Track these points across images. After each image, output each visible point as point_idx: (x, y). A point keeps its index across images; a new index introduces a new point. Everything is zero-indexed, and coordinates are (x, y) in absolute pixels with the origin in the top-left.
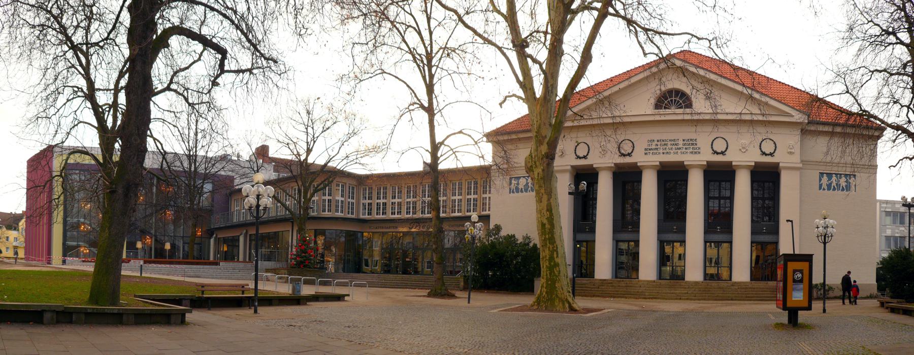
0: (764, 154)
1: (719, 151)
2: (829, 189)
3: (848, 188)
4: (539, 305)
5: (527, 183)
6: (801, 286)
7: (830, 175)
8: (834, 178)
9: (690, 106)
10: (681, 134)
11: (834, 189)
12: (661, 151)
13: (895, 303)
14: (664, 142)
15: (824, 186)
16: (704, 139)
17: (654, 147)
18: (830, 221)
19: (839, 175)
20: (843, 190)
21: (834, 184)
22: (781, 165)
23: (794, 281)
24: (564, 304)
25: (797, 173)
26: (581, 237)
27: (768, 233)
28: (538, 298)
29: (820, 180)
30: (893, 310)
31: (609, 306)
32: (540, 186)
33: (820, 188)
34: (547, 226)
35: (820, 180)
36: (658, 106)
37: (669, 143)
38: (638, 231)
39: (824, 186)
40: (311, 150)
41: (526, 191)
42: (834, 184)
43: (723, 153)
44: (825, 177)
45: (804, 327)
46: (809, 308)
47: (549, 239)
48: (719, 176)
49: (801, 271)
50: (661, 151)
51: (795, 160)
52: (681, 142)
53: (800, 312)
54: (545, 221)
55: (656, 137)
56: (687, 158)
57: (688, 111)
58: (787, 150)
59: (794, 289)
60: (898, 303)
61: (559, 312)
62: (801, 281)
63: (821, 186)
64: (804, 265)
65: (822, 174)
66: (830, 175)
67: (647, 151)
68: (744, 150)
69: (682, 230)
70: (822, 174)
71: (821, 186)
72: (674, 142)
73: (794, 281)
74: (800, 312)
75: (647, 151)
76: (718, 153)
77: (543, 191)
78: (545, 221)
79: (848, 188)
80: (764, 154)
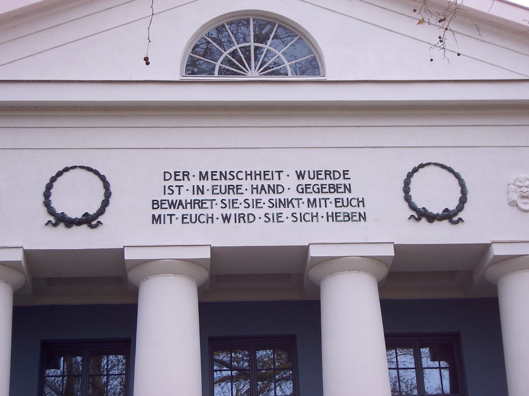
0: (422, 215)
1: (75, 214)
9: (311, 66)
10: (289, 153)
12: (217, 211)
14: (227, 182)
16: (373, 165)
17: (187, 196)
36: (200, 61)
37: (246, 184)
40: (308, 202)
43: (89, 220)
50: (217, 211)
52: (290, 182)
55: (196, 163)
56: (319, 236)
67: (161, 211)
72: (266, 181)
75: (161, 211)
76: (431, 218)
80: (422, 215)
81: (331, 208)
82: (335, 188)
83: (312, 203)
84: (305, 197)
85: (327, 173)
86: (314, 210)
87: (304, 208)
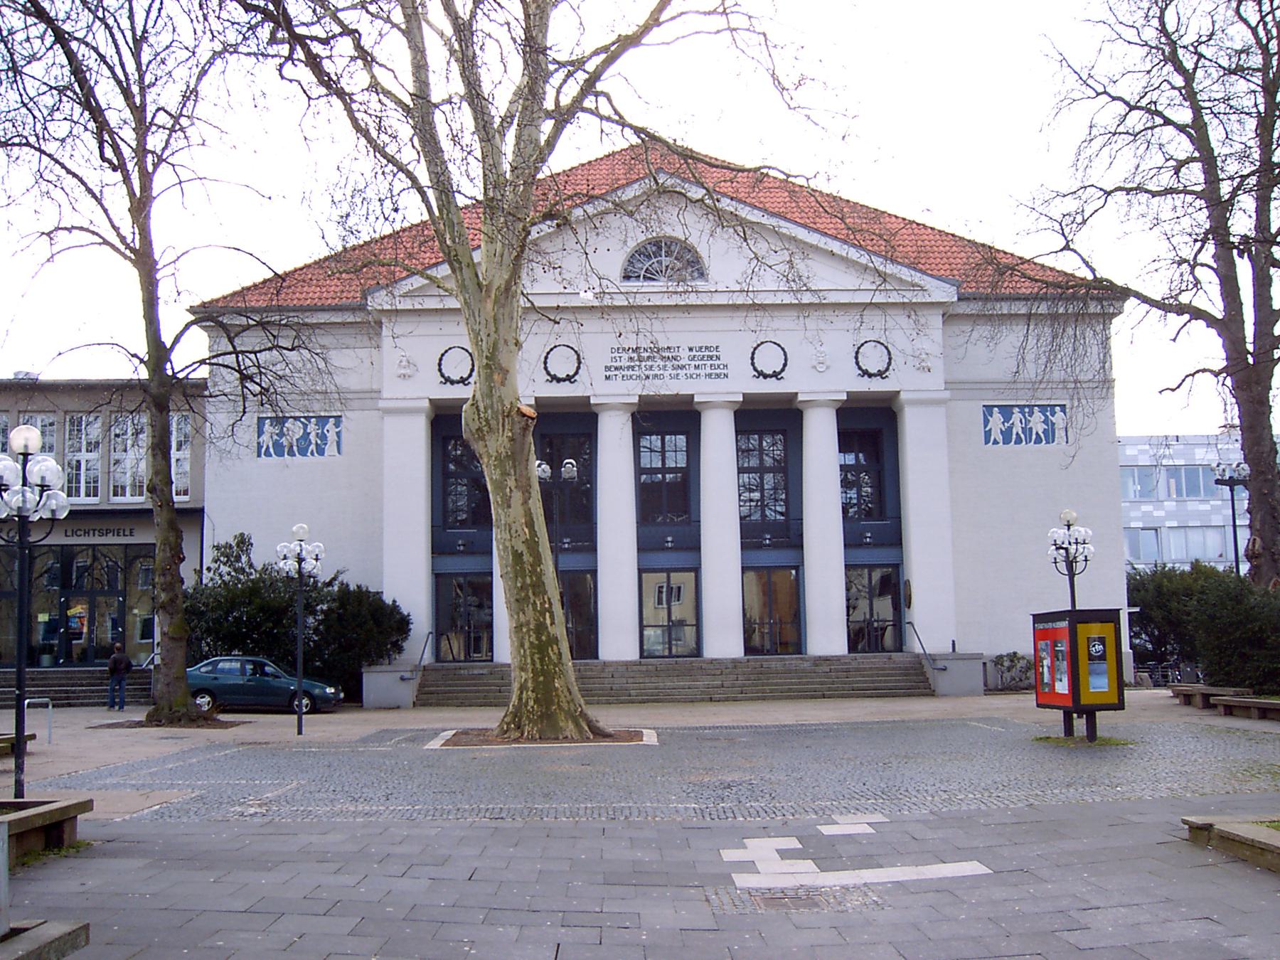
2: (1007, 441)
3: (1049, 435)
4: (515, 728)
5: (306, 435)
6: (1103, 666)
7: (1006, 411)
8: (1017, 416)
11: (1019, 441)
13: (1227, 695)
15: (996, 435)
17: (625, 363)
18: (1080, 531)
19: (1027, 410)
20: (1038, 440)
21: (1018, 429)
22: (903, 396)
23: (1091, 658)
24: (577, 725)
25: (941, 410)
26: (455, 564)
27: (878, 544)
28: (516, 714)
29: (986, 422)
30: (1229, 711)
31: (650, 725)
32: (505, 474)
33: (987, 442)
34: (527, 558)
35: (986, 422)
38: (593, 549)
39: (996, 435)
41: (303, 452)
42: (1018, 429)
44: (997, 417)
45: (1107, 743)
46: (1120, 706)
47: (534, 586)
48: (770, 422)
49: (1102, 641)
51: (933, 383)
52: (684, 354)
53: (1098, 714)
54: (521, 548)
57: (700, 284)
58: (923, 368)
59: (1090, 673)
60: (1237, 695)
61: (573, 740)
62: (1102, 657)
63: (988, 434)
64: (1105, 630)
65: (989, 409)
66: (1006, 411)
68: (821, 366)
69: (694, 545)
70: (989, 409)
71: (988, 434)
73: (1091, 658)
74: (1098, 714)
77: (511, 482)
78: (521, 548)
79: (1049, 435)
81: (708, 371)
82: (711, 358)
83: (697, 367)
84: (693, 363)
85: (707, 348)
86: (698, 372)
87: (692, 370)
